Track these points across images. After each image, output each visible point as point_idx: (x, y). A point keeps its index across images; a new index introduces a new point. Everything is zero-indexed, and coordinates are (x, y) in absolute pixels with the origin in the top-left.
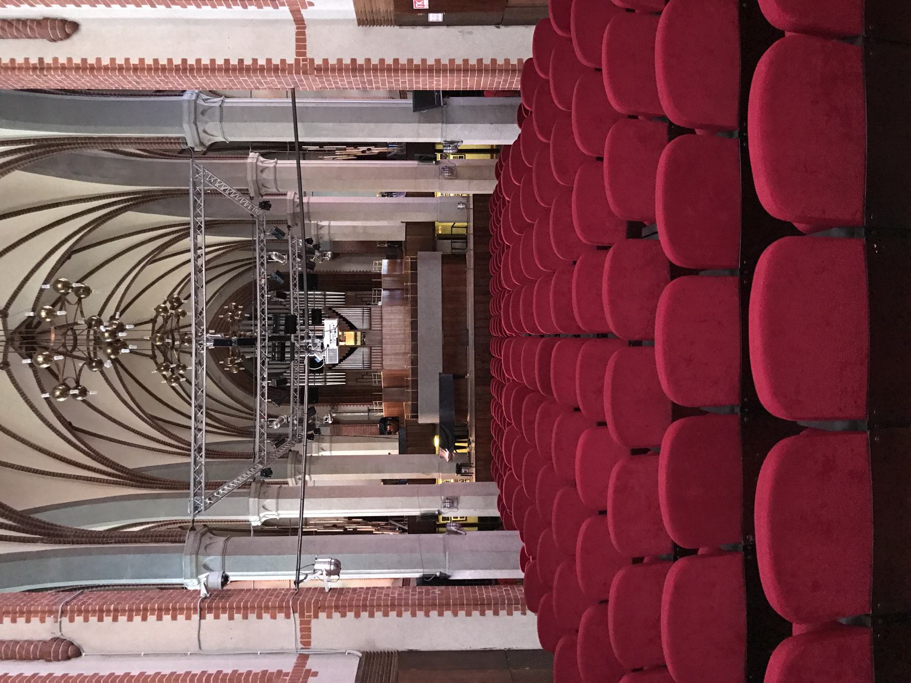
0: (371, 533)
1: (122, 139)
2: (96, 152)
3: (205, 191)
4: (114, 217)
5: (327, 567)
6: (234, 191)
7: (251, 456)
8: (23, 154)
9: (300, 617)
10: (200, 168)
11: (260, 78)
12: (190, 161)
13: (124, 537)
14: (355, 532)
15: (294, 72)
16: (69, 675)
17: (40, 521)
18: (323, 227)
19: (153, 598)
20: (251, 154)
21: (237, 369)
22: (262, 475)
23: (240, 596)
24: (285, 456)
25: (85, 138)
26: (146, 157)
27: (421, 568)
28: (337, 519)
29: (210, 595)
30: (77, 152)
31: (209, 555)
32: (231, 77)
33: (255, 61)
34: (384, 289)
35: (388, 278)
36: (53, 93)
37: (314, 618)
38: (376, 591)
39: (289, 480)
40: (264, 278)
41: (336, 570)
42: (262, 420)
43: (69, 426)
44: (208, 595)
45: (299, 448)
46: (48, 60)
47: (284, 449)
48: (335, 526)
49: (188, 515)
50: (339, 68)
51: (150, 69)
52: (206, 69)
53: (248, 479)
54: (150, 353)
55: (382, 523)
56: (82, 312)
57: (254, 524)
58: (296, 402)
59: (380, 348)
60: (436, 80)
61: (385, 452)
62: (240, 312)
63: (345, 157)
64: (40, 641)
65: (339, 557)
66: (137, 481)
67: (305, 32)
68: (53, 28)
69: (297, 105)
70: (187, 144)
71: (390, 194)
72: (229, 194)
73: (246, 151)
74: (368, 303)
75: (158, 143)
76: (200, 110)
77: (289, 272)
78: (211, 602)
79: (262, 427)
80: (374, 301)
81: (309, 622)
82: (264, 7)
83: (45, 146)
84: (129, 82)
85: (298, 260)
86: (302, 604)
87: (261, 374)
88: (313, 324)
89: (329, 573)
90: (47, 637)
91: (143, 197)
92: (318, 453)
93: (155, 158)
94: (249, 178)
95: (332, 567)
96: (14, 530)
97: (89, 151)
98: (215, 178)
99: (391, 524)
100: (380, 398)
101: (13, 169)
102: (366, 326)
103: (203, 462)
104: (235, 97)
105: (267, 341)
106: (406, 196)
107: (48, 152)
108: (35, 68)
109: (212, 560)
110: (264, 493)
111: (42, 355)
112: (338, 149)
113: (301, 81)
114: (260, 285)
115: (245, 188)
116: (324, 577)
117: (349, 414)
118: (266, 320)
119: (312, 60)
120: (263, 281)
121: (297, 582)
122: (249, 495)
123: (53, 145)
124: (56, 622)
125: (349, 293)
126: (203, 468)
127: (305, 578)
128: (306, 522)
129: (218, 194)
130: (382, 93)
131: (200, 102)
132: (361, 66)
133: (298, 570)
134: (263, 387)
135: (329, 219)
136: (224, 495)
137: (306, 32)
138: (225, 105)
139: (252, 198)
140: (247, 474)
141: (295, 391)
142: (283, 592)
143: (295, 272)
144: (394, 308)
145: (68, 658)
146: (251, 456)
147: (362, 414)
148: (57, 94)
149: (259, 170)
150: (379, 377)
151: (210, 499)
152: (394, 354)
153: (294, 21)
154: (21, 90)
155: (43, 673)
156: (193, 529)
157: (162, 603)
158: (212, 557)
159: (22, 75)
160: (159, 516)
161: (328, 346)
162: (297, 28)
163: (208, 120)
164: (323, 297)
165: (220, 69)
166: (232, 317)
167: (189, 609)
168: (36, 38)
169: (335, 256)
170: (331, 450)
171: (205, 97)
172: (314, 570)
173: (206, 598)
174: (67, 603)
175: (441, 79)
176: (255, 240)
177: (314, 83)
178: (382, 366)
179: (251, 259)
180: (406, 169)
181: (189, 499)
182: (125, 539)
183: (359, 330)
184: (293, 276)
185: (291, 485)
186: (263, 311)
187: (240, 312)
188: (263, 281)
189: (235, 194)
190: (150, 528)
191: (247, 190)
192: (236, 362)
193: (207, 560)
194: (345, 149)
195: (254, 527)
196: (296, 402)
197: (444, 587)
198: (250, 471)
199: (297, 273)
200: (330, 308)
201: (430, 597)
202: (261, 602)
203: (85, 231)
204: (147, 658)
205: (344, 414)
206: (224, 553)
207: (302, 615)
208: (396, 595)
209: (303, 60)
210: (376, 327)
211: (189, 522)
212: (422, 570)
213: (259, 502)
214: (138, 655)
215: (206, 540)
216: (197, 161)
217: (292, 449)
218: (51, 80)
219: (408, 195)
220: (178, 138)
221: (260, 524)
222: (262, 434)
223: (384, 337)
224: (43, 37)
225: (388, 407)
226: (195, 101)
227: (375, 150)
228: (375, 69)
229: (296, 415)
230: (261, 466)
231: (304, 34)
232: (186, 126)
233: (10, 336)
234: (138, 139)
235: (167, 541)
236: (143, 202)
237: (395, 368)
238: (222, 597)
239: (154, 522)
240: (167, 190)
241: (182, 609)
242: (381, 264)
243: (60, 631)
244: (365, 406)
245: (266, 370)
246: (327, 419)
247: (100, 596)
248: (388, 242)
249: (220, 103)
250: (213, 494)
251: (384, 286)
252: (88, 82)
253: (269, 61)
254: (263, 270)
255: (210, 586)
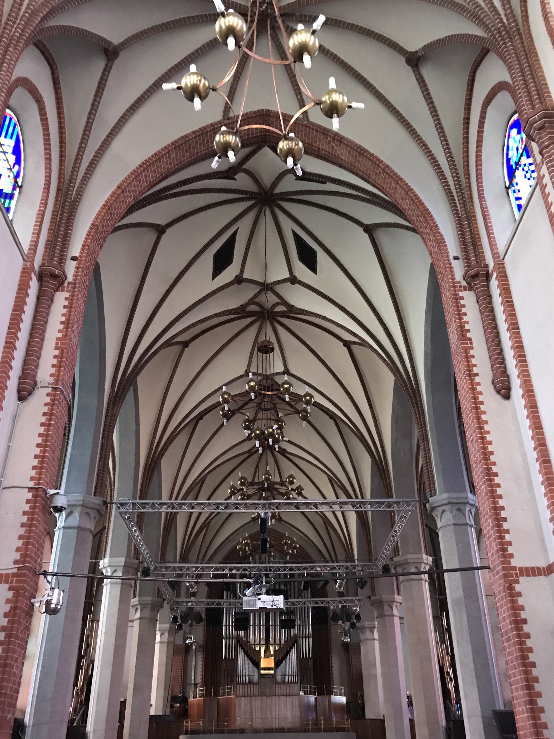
0: (76, 684)
1: (428, 447)
2: (416, 433)
3: (394, 511)
4: (366, 448)
5: (54, 601)
6: (396, 540)
7: (163, 559)
8: (406, 380)
9: (13, 574)
10: (412, 507)
11: (494, 537)
12: (417, 499)
13: (105, 455)
14: (79, 667)
15: (504, 565)
16: (6, 391)
17: (127, 391)
18: (372, 632)
19: (54, 453)
20: (430, 559)
21: (240, 549)
22: (145, 568)
23: (41, 522)
24: (159, 593)
25: (424, 421)
26: (417, 472)
27: (33, 723)
28: (94, 649)
29: (47, 498)
30: (414, 420)
31: (80, 515)
32: (490, 512)
33: (508, 531)
34: (316, 698)
35: (327, 703)
36: (456, 400)
37: (10, 586)
38: (23, 649)
39: (137, 599)
40: (321, 570)
41: (51, 611)
42: (194, 569)
43: (200, 417)
44: (48, 496)
45: (166, 606)
46: (465, 318)
47: (168, 592)
48: (88, 646)
49: (118, 499)
50: (516, 609)
51: (485, 449)
52: (493, 491)
53: (143, 556)
54: (256, 481)
55: (83, 698)
56: (288, 414)
57: (101, 562)
58: (208, 604)
59: (257, 694)
60: (523, 709)
61: (153, 701)
62: (290, 551)
63: (440, 654)
64: (46, 328)
65: (61, 615)
66: (150, 465)
67: (542, 575)
68: (502, 382)
69: (476, 571)
70: (431, 497)
71: (410, 704)
72: (393, 536)
73: (432, 554)
74: (302, 682)
75: (428, 475)
76: (462, 507)
77: (328, 597)
78: (42, 497)
79: (188, 569)
80: (304, 687)
81: (6, 582)
82: (546, 498)
83: (414, 394)
84: (471, 435)
85: (340, 606)
86: (25, 575)
87: (235, 568)
88: (281, 621)
89: (48, 603)
90: (38, 379)
91: (383, 469)
92: (159, 630)
93: (417, 481)
94: (409, 556)
95: (53, 606)
96: (124, 371)
97: (416, 427)
98: (405, 522)
99: (80, 709)
100: (208, 694)
101: (394, 374)
102: (279, 678)
103: (161, 510)
104: (479, 551)
105: (265, 573)
106: (410, 720)
107: (410, 397)
108: (470, 371)
109: (76, 517)
110: (128, 571)
111: (255, 385)
112: (447, 646)
113: (498, 573)
114: (315, 566)
115: (400, 553)
116: (46, 598)
117: (194, 663)
118: (284, 572)
119: (518, 582)
120: (319, 569)
121: (45, 574)
122: (128, 557)
123: (416, 400)
124: (49, 384)
125: (311, 663)
126: (157, 510)
127: (48, 581)
128: (101, 580)
129: (392, 524)
130: (508, 695)
131: (468, 508)
132: (522, 629)
133: (56, 574)
134: (223, 570)
135: (381, 641)
136: (131, 531)
137: (541, 576)
138: (469, 528)
139: (392, 559)
140: (147, 554)
141: (219, 604)
142: (39, 560)
143: (329, 603)
144: (297, 709)
145: (19, 391)
146: (163, 559)
147: (193, 677)
148: (456, 403)
149: (417, 565)
150: (229, 694)
151: (128, 518)
152: (251, 709)
153: (549, 565)
154: (455, 380)
155: (11, 373)
156: (105, 503)
157: (49, 459)
158: (78, 519)
159: (463, 363)
160: (119, 482)
161: (259, 599)
162: (543, 568)
163: (454, 514)
164: (307, 635)
165: (495, 503)
166: (286, 543)
167: (39, 479)
168: (493, 371)
169: (346, 646)
170: (160, 642)
171: (473, 511)
172: (53, 589)
173: (46, 493)
174: (62, 392)
175: (526, 715)
176: (354, 562)
177: (499, 586)
178: (239, 696)
179: (336, 557)
180: (436, 712)
181: (131, 499)
182: (104, 450)
183: (275, 672)
184: (324, 601)
185: (132, 600)
186: (291, 569)
187: (290, 551)
188: (319, 569)
189: (394, 540)
190: (110, 475)
191: (399, 555)
192: (247, 548)
193: (76, 515)
194: (448, 654)
195: (99, 562)
196: (208, 604)
197: (12, 724)
198: (149, 558)
199: (326, 605)
200: (296, 641)
201: (6, 707)
202: (34, 539)
203: (352, 427)
204: (6, 447)
205: (194, 658)
206: (80, 528)
207: (14, 575)
208: (14, 670)
209: (516, 574)
210: (278, 690)
211: (111, 499)
212: (31, 724)
213: (120, 566)
214: (10, 440)
215: (93, 514)
216: (418, 504)
217: (165, 602)
218: (463, 382)
219: (412, 721)
220: (435, 490)
221: (100, 567)
222: (181, 569)
223: (269, 698)
224: (494, 375)
225: (198, 704)
226: (468, 503)
227: (451, 686)
228: (521, 643)
229: (197, 605)
230: (152, 568)
231: (540, 574)
232: (446, 495)
233: (270, 377)
234: (430, 459)
235: (97, 483)
236: (379, 469)
237: (237, 711)
238: (43, 506)
239: (114, 479)
240: (391, 487)
241: (40, 474)
242: (341, 695)
243: (41, 387)
244: (201, 681)
245: (239, 572)
246: (191, 638)
247: (63, 415)
248: (363, 704)
249: (469, 523)
250: (133, 521)
251: (320, 698)
252: (466, 406)
253: (510, 543)
254: (329, 569)
255: (56, 496)
